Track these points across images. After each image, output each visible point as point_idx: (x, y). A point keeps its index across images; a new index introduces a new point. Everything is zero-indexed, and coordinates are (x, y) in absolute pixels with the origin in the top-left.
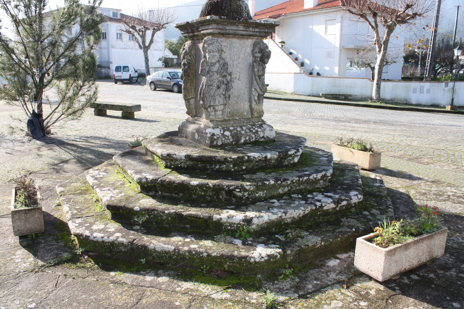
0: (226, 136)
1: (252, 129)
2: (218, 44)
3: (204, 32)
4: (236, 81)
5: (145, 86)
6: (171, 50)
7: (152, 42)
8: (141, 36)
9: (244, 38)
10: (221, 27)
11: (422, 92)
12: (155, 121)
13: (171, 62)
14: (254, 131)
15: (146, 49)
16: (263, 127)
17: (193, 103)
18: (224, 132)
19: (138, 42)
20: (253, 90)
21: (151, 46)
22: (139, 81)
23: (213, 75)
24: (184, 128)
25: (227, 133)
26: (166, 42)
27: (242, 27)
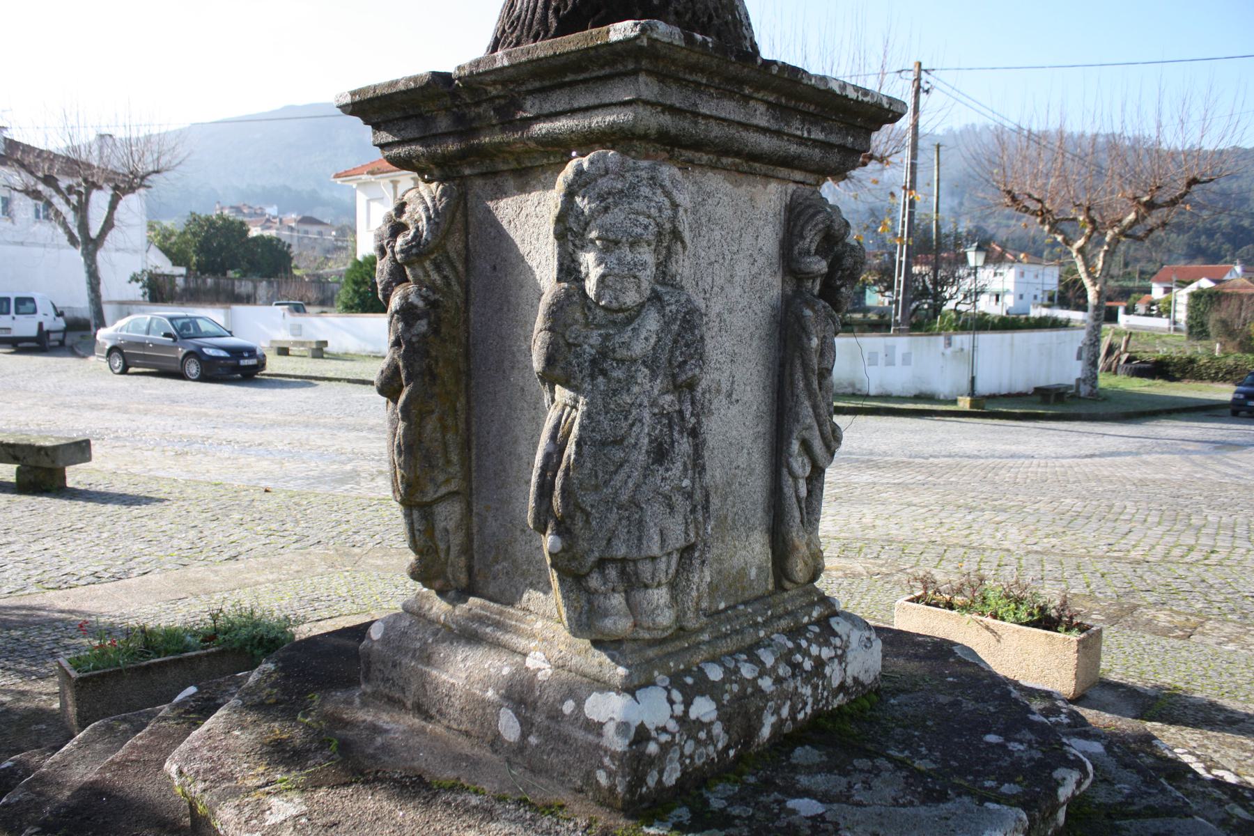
0: (700, 724)
1: (799, 658)
2: (660, 198)
3: (562, 125)
4: (719, 403)
5: (92, 359)
6: (166, 251)
7: (108, 224)
8: (75, 209)
9: (753, 173)
10: (675, 98)
11: (890, 363)
12: (148, 500)
13: (168, 287)
14: (808, 665)
15: (90, 245)
16: (835, 634)
17: (451, 525)
18: (688, 703)
19: (64, 225)
20: (795, 446)
21: (108, 237)
22: (68, 341)
23: (631, 379)
24: (409, 662)
25: (703, 708)
26: (151, 227)
27: (762, 108)
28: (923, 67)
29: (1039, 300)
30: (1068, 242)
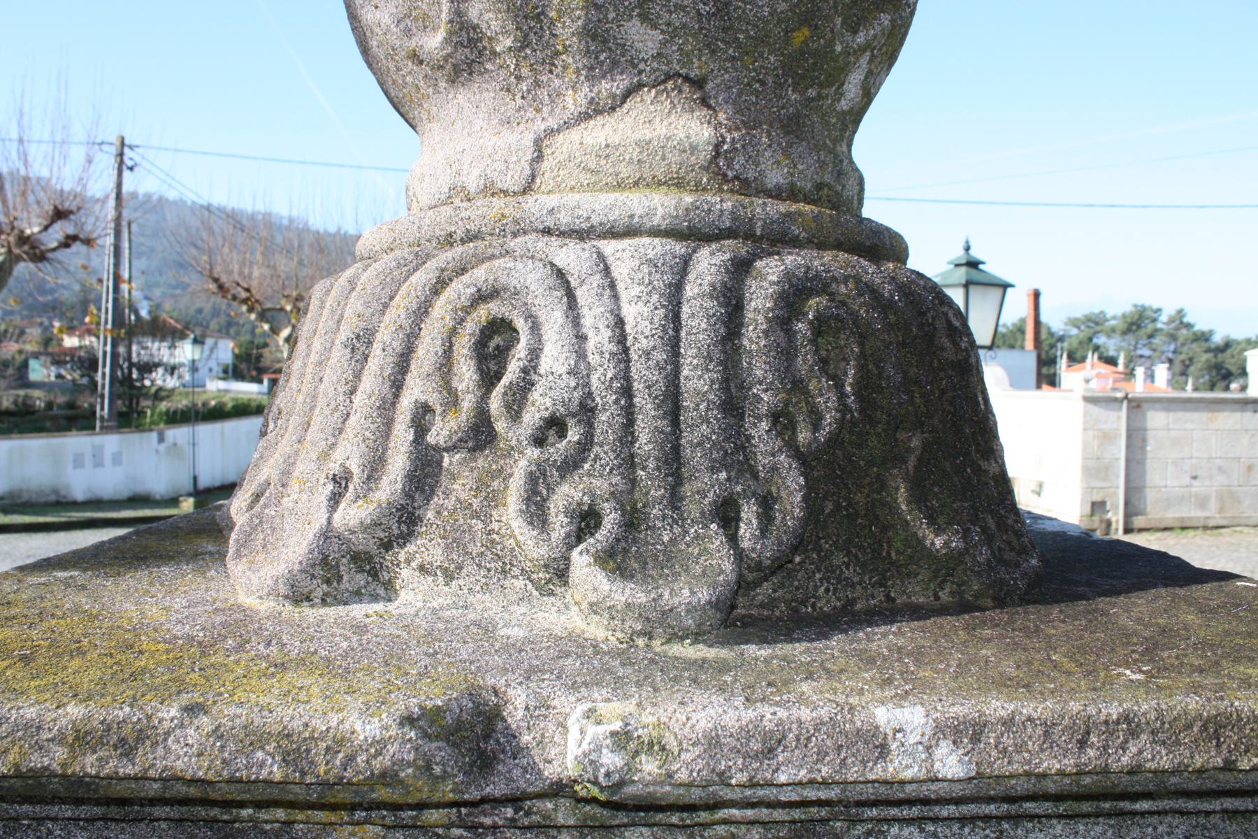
28: (127, 142)
29: (214, 373)
30: (275, 331)
